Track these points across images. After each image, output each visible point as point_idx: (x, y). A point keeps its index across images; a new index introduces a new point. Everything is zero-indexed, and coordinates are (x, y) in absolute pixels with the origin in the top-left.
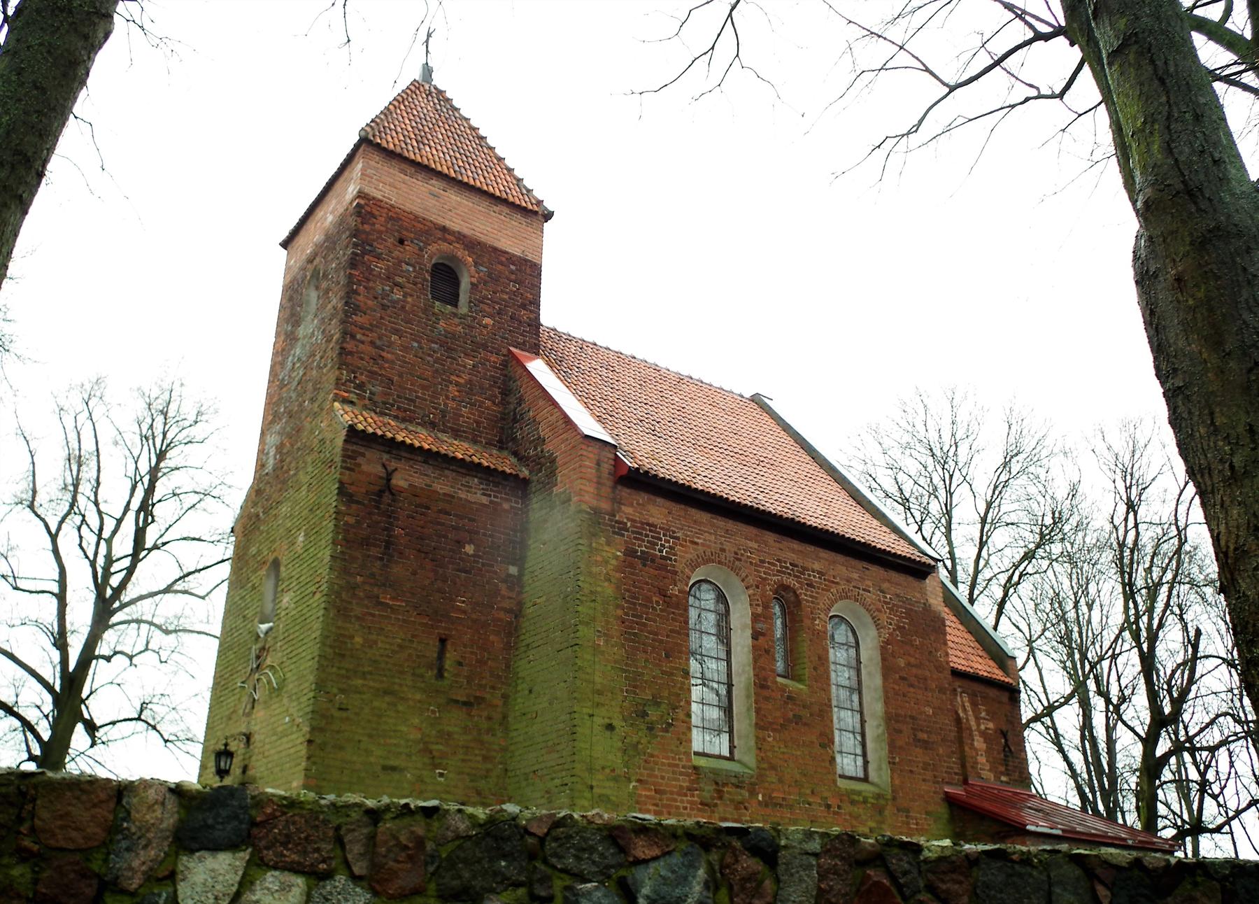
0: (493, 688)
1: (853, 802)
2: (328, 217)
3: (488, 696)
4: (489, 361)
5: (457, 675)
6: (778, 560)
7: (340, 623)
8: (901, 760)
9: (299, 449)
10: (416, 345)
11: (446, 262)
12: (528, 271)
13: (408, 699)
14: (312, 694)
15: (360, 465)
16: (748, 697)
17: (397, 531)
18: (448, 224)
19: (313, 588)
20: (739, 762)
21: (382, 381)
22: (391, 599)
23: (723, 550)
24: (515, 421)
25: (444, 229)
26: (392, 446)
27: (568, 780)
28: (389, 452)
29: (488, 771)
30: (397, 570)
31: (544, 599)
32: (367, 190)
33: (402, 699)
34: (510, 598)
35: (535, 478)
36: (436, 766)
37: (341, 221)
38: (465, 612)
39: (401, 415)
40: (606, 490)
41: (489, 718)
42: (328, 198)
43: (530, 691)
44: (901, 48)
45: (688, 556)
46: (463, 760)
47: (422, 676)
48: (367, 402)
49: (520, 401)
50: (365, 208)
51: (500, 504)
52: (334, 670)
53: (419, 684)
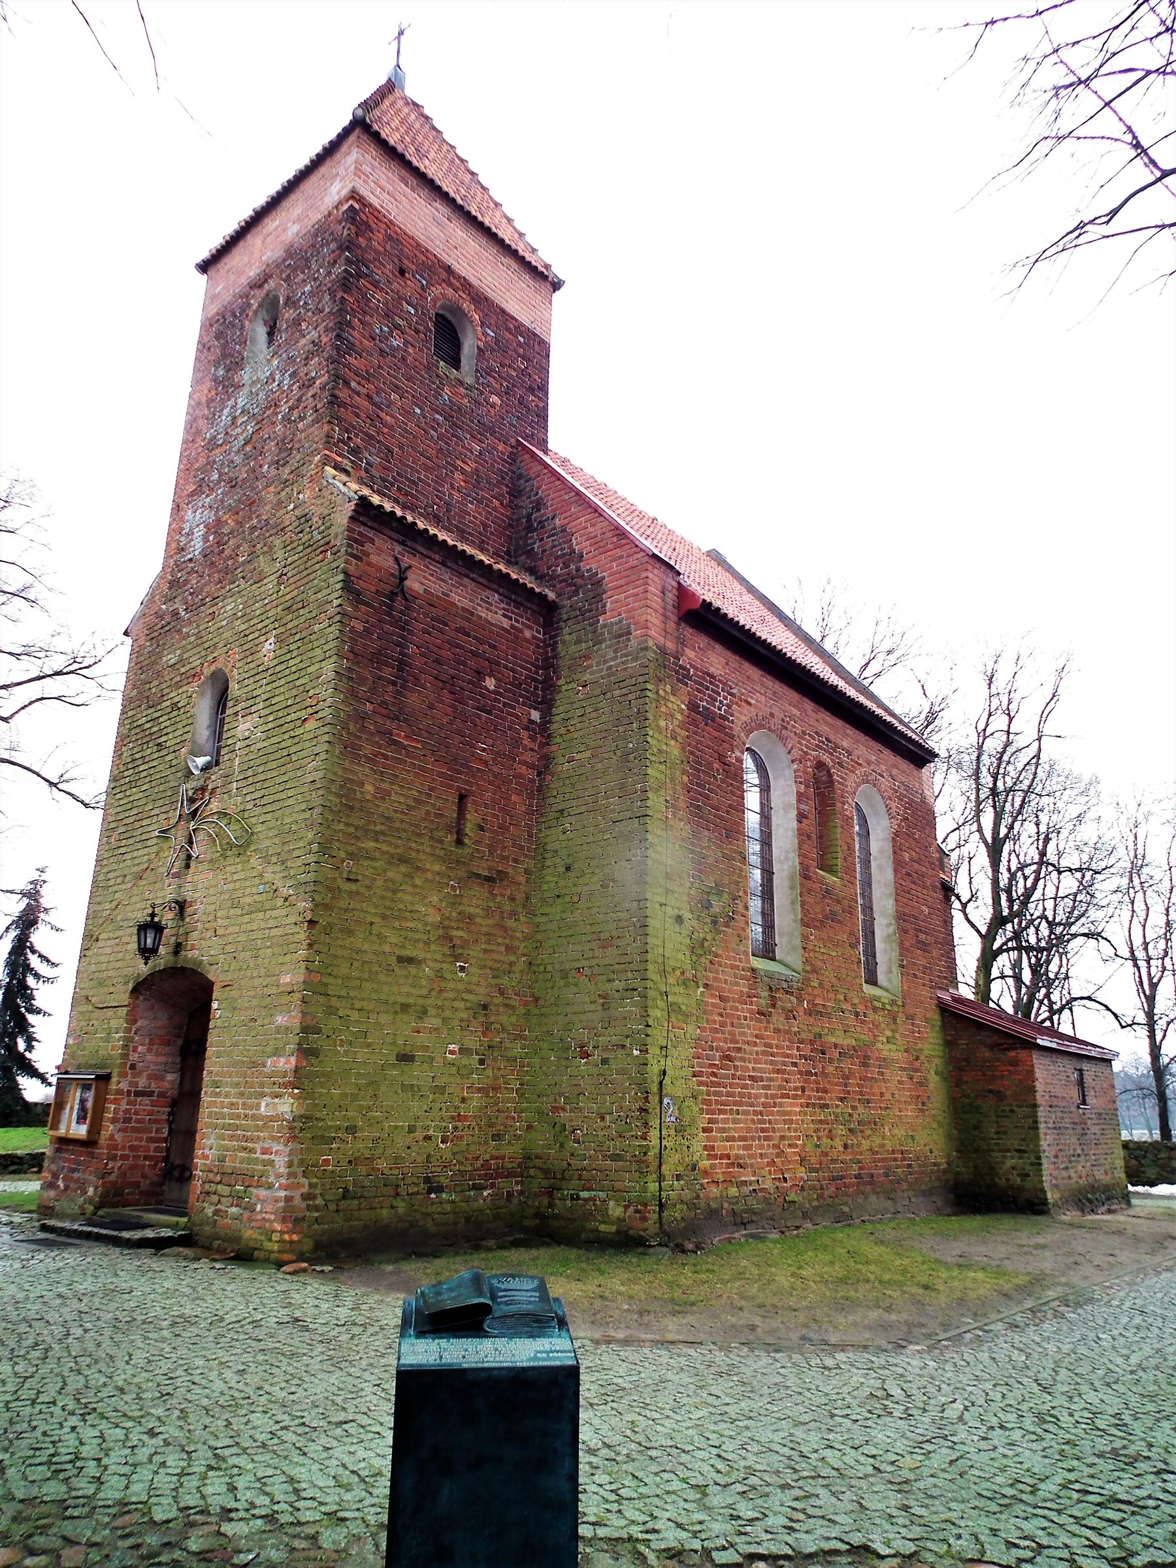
0: (516, 861)
1: (875, 1009)
2: (290, 226)
3: (510, 871)
4: (496, 449)
5: (477, 842)
6: (817, 733)
7: (347, 764)
8: (908, 962)
9: (254, 528)
10: (418, 411)
11: (448, 315)
12: (537, 348)
13: (425, 871)
14: (311, 858)
15: (368, 555)
16: (792, 888)
17: (412, 649)
18: (456, 267)
19: (303, 714)
20: (781, 962)
21: (380, 451)
22: (407, 737)
23: (772, 715)
24: (530, 528)
25: (449, 269)
26: (407, 534)
27: (636, 983)
28: (402, 543)
29: (512, 964)
30: (413, 700)
31: (588, 754)
32: (364, 192)
33: (418, 868)
34: (532, 750)
35: (567, 603)
36: (457, 958)
37: (321, 230)
38: (486, 763)
39: (402, 499)
40: (671, 625)
41: (512, 899)
42: (286, 204)
43: (568, 869)
44: (1107, 104)
45: (744, 718)
46: (486, 951)
47: (441, 842)
48: (363, 474)
49: (539, 505)
50: (358, 215)
51: (521, 631)
52: (341, 826)
53: (437, 852)
